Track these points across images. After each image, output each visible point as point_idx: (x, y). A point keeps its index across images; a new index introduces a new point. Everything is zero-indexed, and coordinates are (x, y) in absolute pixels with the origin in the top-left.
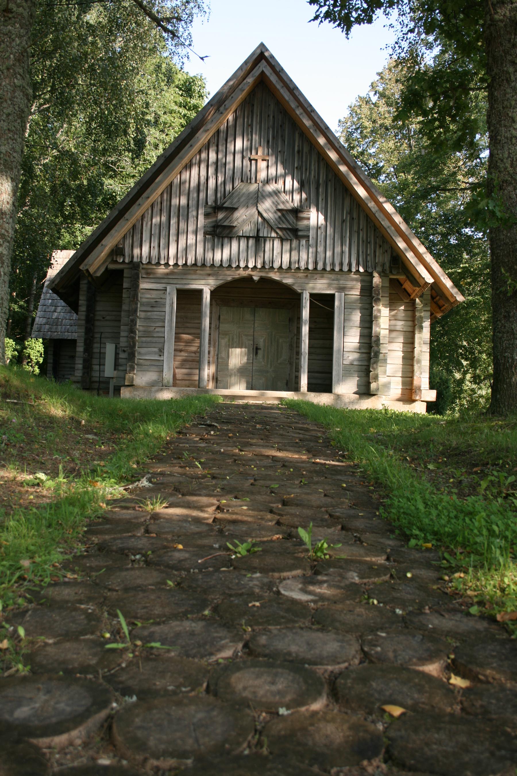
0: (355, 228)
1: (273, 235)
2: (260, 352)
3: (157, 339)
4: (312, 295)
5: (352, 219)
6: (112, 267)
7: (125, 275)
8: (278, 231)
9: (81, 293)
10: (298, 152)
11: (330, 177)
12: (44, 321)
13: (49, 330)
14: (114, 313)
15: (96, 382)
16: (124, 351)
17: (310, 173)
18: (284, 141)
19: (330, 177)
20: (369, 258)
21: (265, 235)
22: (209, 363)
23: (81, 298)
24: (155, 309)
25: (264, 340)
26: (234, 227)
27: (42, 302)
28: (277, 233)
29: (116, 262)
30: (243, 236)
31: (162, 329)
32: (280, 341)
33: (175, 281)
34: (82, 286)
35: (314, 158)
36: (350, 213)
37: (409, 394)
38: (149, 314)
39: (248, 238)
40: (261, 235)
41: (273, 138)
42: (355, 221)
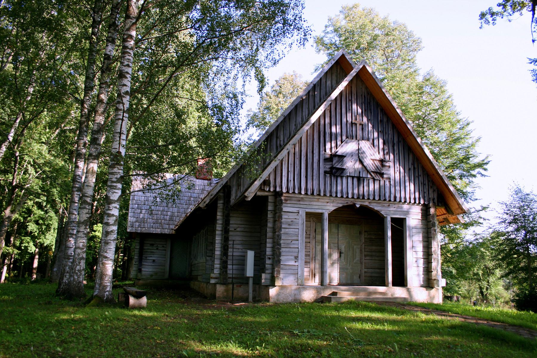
0: (417, 175)
1: (369, 176)
2: (342, 255)
3: (293, 249)
4: (392, 218)
5: (414, 168)
6: (259, 194)
7: (270, 200)
8: (372, 174)
9: (218, 210)
10: (381, 121)
11: (400, 139)
12: (135, 219)
13: (139, 226)
14: (243, 226)
15: (230, 278)
16: (269, 258)
17: (388, 136)
18: (371, 112)
19: (400, 139)
20: (425, 195)
21: (364, 176)
22: (371, 277)
23: (219, 214)
24: (291, 227)
25: (345, 247)
26: (344, 169)
27: (130, 206)
28: (371, 175)
29: (264, 190)
30: (350, 176)
31: (297, 242)
32: (355, 247)
33: (305, 206)
34: (219, 205)
35: (390, 125)
36: (413, 164)
37: (429, 284)
38: (287, 230)
39: (353, 177)
40: (361, 176)
41: (365, 110)
42: (416, 170)
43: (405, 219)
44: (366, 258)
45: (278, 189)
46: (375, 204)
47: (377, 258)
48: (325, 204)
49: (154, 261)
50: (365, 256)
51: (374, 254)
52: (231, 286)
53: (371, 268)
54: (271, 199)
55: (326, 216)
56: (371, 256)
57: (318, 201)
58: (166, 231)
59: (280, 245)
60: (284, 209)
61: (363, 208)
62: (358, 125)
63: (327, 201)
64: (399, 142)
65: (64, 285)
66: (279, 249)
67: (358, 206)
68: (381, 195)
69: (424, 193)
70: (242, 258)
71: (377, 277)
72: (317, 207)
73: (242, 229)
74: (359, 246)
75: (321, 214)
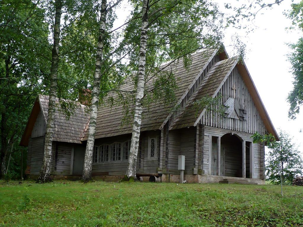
4: (246, 141)
5: (256, 115)
7: (197, 129)
43: (132, 133)
44: (226, 163)
45: (201, 123)
46: (239, 134)
47: (230, 163)
48: (219, 132)
49: (63, 162)
50: (225, 162)
51: (229, 161)
52: (168, 175)
53: (229, 169)
54: (198, 128)
55: (220, 139)
56: (228, 162)
57: (217, 131)
58: (76, 142)
59: (203, 153)
60: (205, 134)
61: (235, 136)
62: (234, 90)
63: (220, 130)
64: (250, 101)
65: (46, 175)
66: (203, 155)
67: (233, 134)
68: (243, 129)
69: (260, 129)
70: (175, 160)
71: (230, 174)
72: (216, 134)
73: (172, 143)
74: (223, 156)
75: (218, 137)
